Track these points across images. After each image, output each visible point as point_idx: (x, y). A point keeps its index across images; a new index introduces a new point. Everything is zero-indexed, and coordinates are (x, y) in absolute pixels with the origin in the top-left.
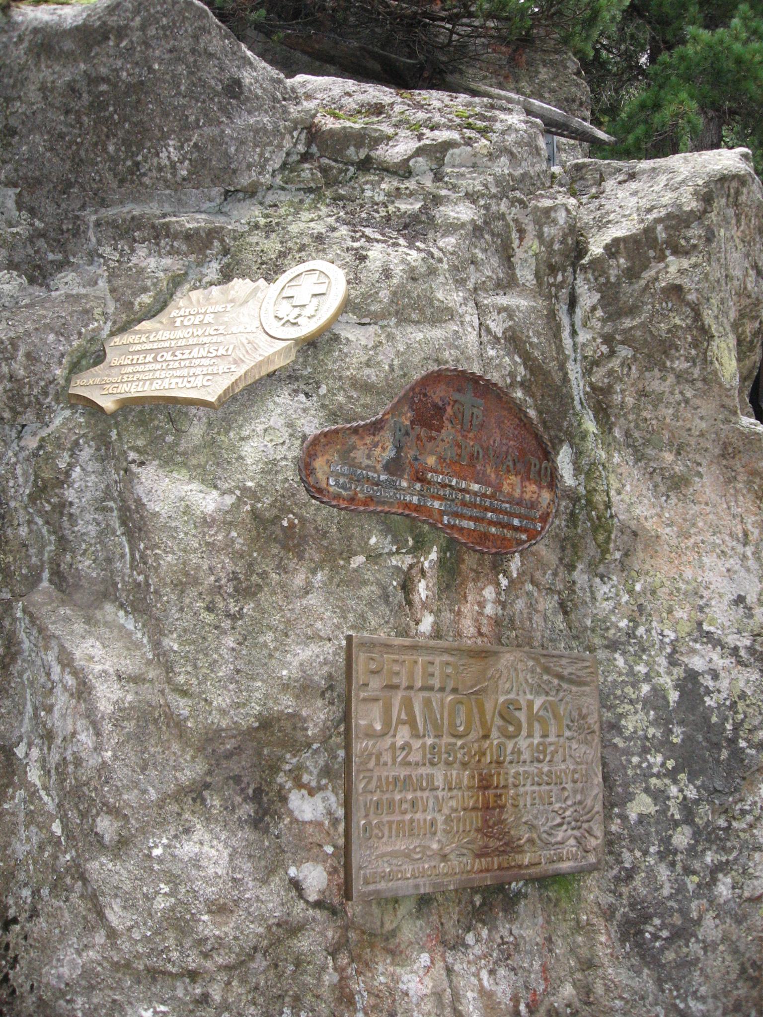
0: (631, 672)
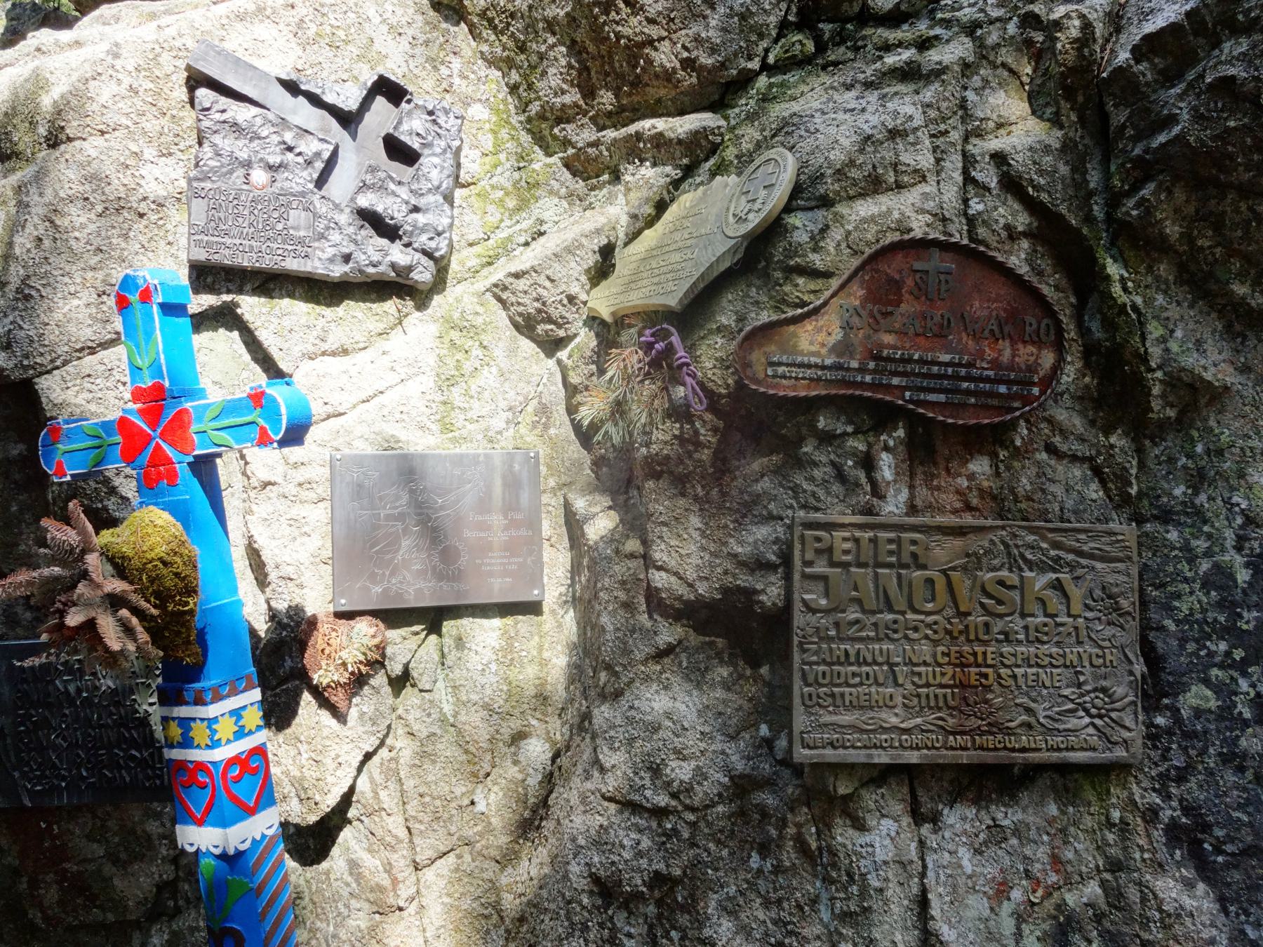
0: (1186, 548)
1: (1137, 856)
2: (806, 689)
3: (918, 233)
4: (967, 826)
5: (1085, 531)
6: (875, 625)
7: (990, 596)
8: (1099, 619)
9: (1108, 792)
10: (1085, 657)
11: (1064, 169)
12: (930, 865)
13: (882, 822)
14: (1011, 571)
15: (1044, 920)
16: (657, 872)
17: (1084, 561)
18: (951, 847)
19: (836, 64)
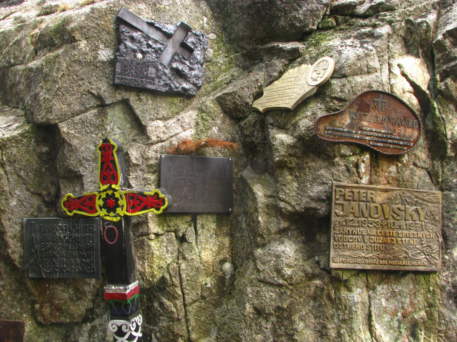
1: (438, 302)
2: (335, 243)
3: (375, 89)
4: (384, 291)
5: (425, 192)
6: (358, 221)
7: (395, 213)
8: (429, 222)
9: (429, 280)
10: (424, 235)
12: (372, 304)
13: (358, 289)
14: (402, 205)
15: (407, 323)
16: (278, 306)
17: (425, 203)
18: (379, 298)
19: (342, 30)
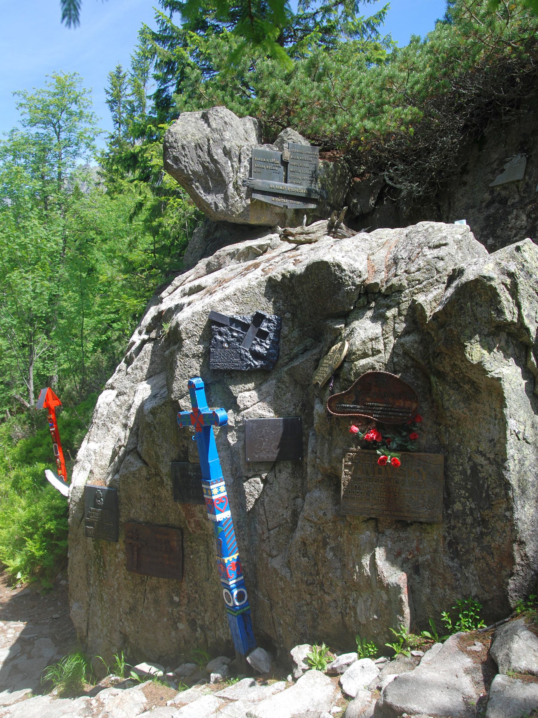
11: (421, 348)
